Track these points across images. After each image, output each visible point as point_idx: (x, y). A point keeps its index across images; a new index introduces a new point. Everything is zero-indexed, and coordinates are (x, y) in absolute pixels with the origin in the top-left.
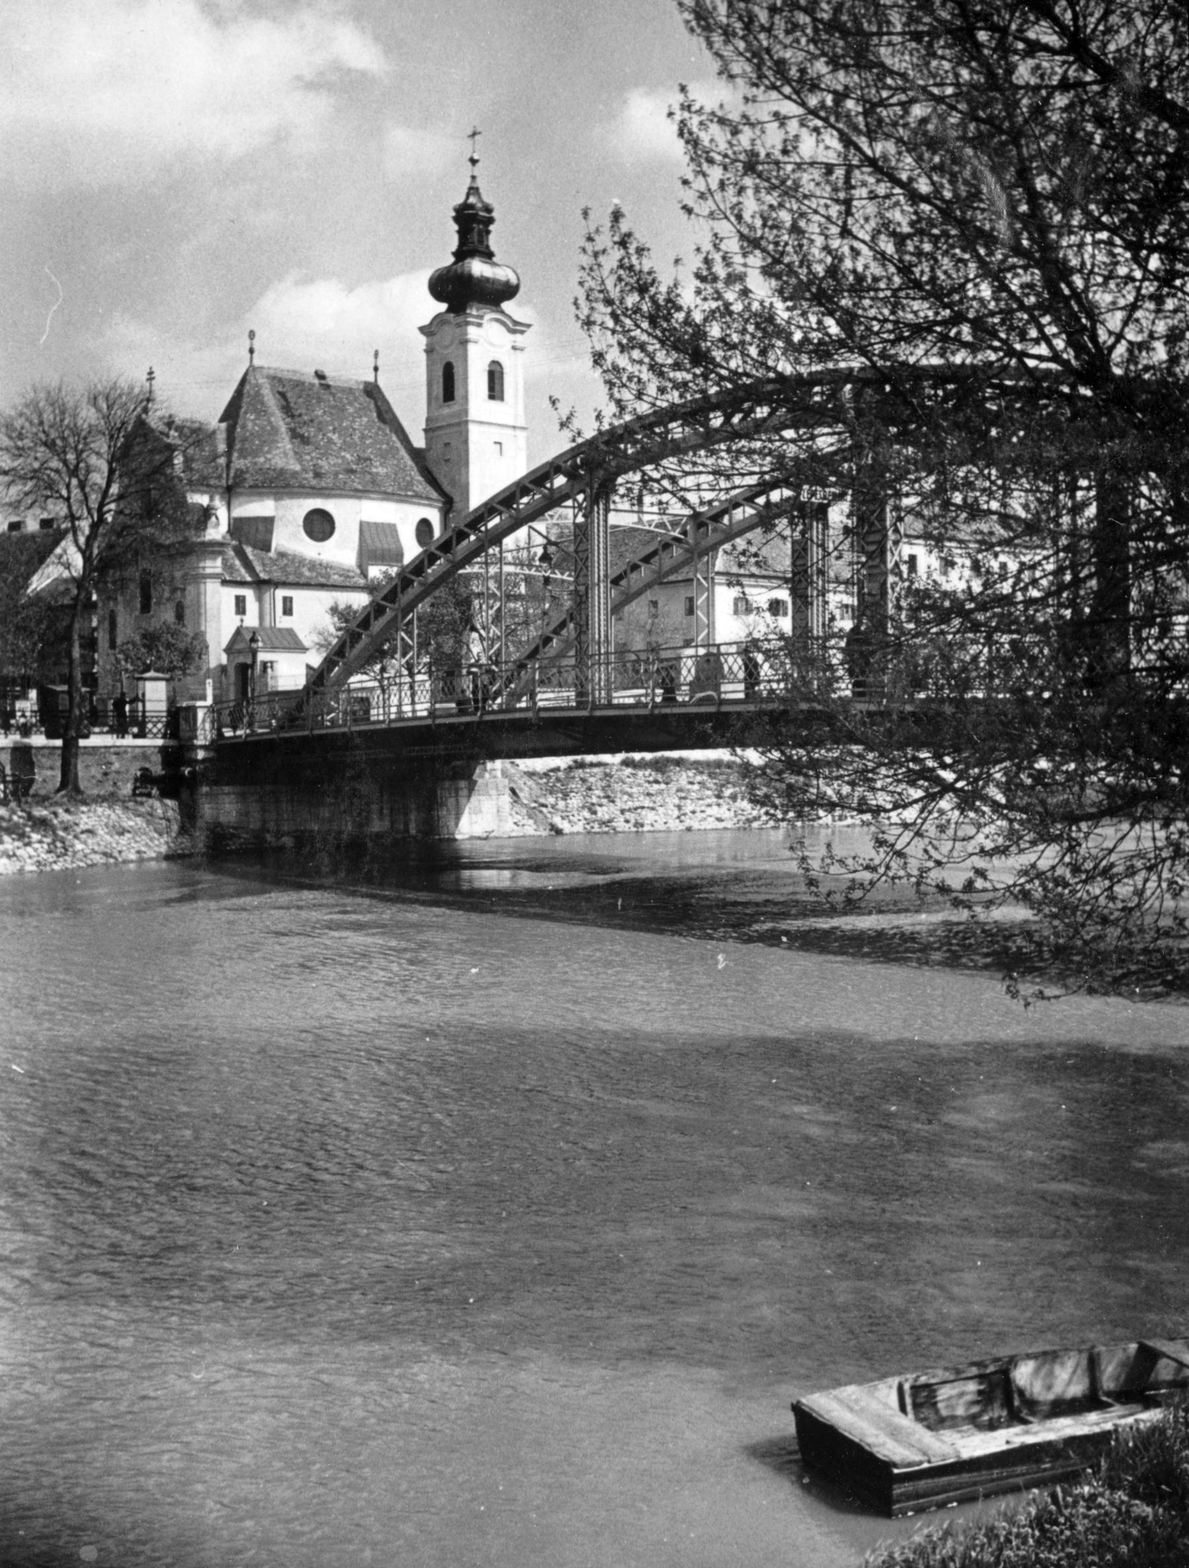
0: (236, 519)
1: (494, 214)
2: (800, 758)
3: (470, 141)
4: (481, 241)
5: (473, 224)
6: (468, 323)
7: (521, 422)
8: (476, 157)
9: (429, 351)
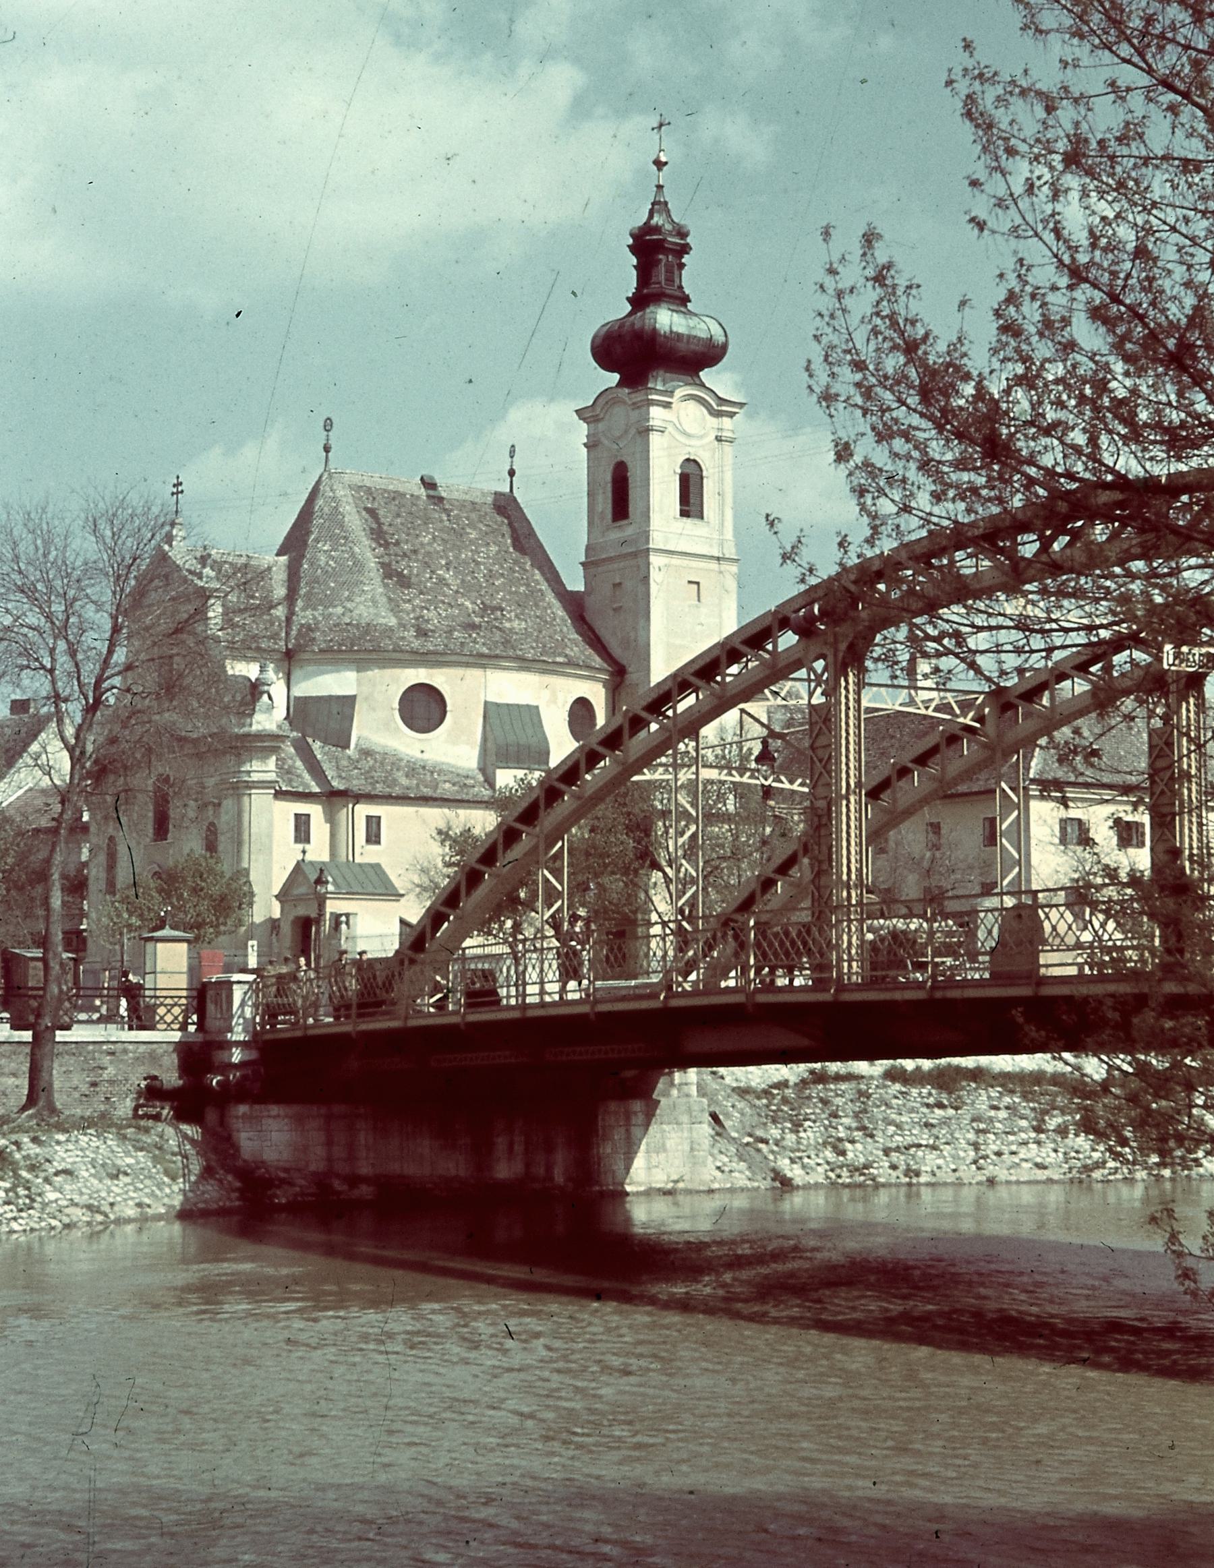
4: (670, 280)
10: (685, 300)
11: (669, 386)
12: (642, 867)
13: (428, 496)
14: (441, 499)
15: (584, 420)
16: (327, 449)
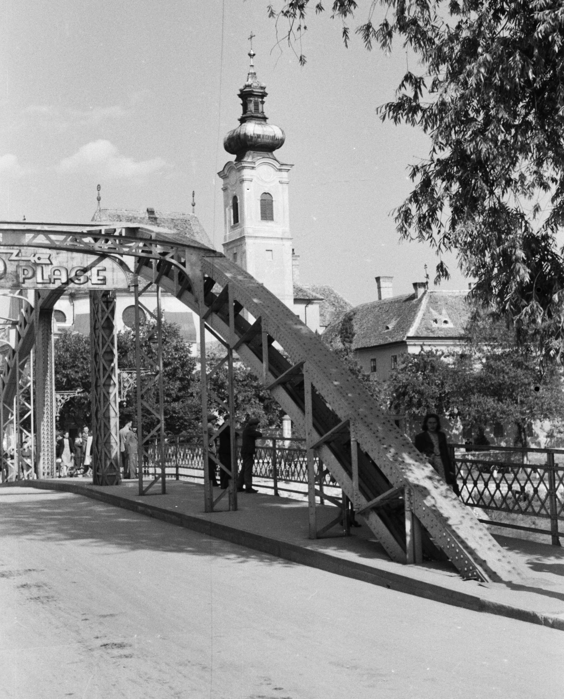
0: (77, 315)
1: (267, 91)
2: (520, 38)
3: (249, 41)
4: (257, 109)
5: (251, 100)
6: (244, 168)
7: (290, 237)
8: (252, 53)
9: (225, 189)
10: (265, 119)
11: (254, 160)
12: (215, 408)
13: (149, 218)
14: (156, 219)
15: (221, 177)
16: (99, 199)
